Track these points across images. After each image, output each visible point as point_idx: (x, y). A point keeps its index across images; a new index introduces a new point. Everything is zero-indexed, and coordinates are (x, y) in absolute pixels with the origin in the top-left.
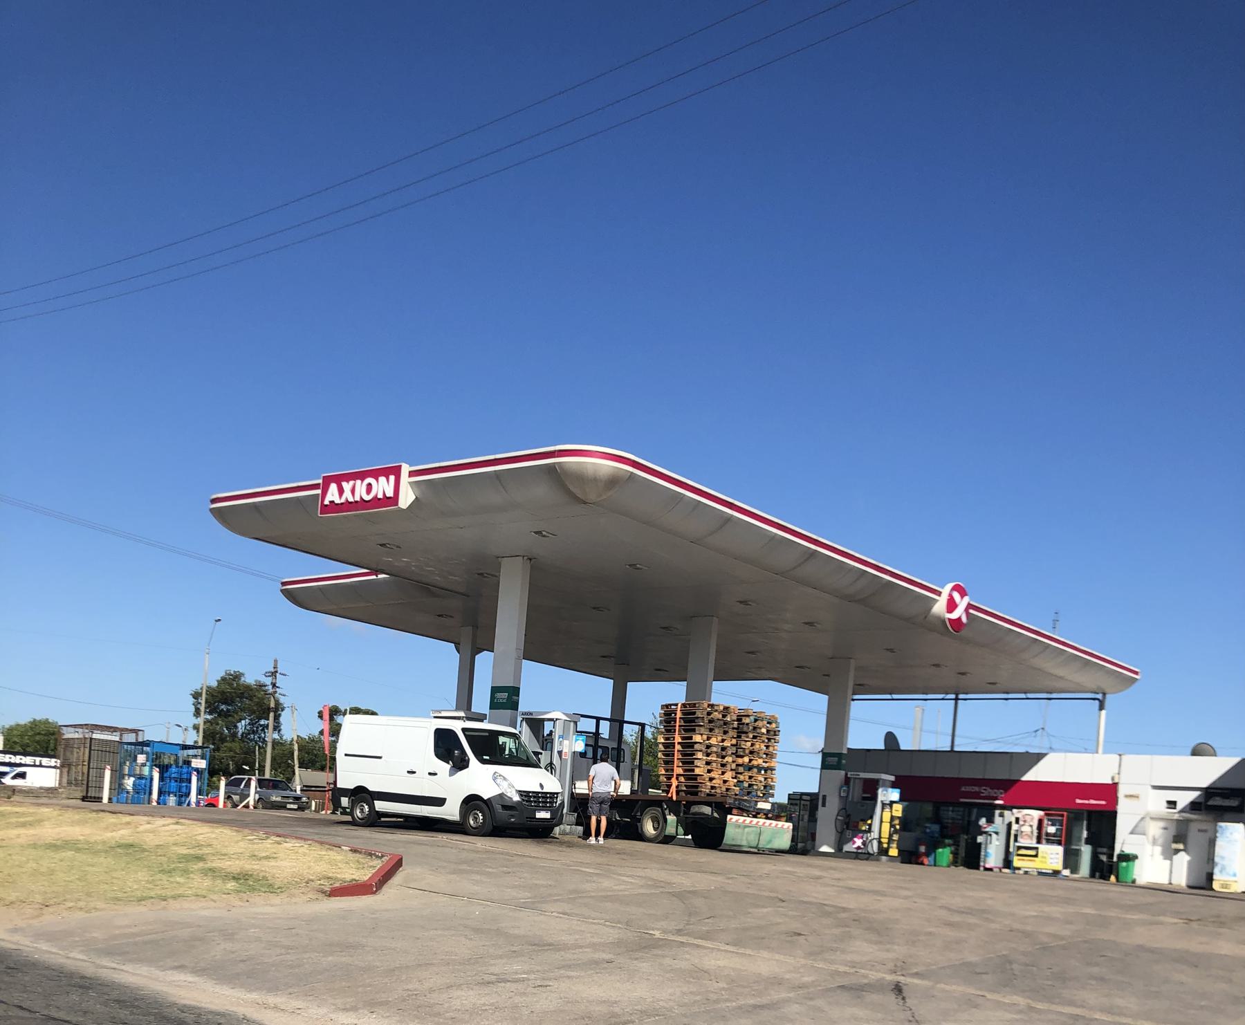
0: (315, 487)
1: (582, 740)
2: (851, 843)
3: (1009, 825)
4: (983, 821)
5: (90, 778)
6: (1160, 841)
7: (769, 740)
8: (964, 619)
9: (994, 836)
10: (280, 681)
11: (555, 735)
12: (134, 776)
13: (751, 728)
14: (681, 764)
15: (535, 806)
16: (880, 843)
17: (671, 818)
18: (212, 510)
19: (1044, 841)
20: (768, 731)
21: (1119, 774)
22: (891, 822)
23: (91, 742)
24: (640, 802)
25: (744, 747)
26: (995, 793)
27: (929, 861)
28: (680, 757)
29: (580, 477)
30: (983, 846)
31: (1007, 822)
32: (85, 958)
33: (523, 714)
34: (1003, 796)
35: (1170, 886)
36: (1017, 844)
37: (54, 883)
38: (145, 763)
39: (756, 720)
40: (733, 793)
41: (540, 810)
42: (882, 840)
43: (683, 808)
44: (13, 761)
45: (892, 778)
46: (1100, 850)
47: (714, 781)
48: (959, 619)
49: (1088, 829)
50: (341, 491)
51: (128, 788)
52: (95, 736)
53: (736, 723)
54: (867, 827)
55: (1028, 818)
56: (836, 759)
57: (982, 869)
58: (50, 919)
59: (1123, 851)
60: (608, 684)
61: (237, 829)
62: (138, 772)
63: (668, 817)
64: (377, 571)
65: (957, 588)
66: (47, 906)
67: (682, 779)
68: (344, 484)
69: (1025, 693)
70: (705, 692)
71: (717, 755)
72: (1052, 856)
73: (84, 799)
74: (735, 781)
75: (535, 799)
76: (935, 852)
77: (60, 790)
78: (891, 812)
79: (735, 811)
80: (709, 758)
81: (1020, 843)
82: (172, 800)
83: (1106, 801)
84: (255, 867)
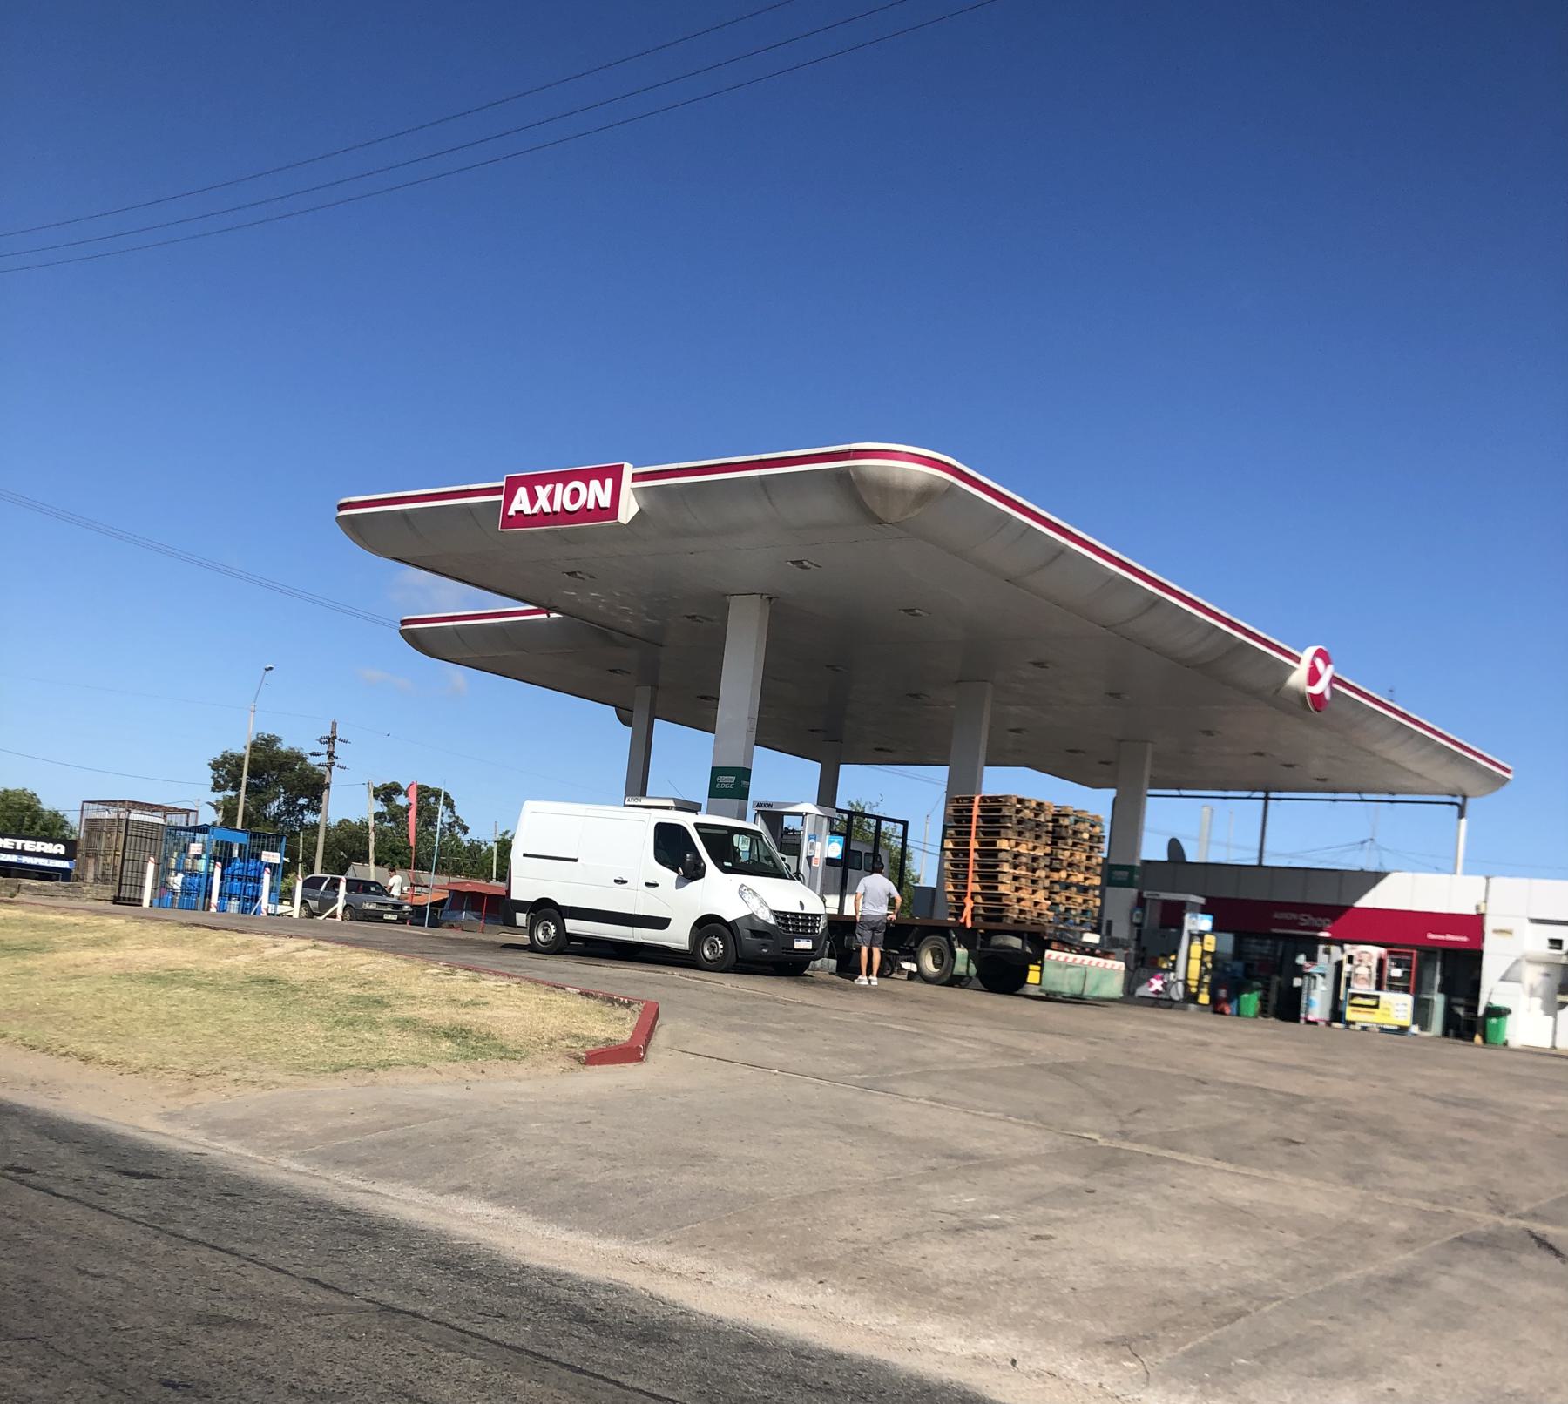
0: (497, 491)
1: (839, 842)
2: (1146, 985)
3: (1339, 965)
4: (1301, 959)
5: (124, 874)
6: (1540, 991)
7: (1092, 848)
8: (1328, 695)
9: (1320, 979)
10: (339, 749)
11: (804, 835)
12: (183, 872)
13: (1071, 832)
14: (977, 879)
15: (794, 932)
16: (1186, 986)
17: (961, 952)
18: (338, 519)
19: (1385, 987)
20: (1091, 837)
21: (1485, 902)
22: (1201, 959)
23: (127, 824)
24: (917, 928)
25: (1061, 857)
26: (1319, 922)
27: (1231, 1009)
28: (977, 869)
29: (884, 488)
30: (1305, 992)
31: (1334, 960)
32: (302, 1168)
33: (758, 805)
34: (1329, 926)
35: (1554, 1051)
36: (1350, 991)
37: (189, 1038)
38: (201, 855)
39: (1076, 822)
40: (1046, 920)
41: (799, 938)
42: (1190, 983)
43: (979, 939)
44: (45, 850)
45: (1202, 901)
46: (1455, 1000)
47: (1023, 903)
48: (1322, 695)
49: (1442, 974)
50: (533, 498)
51: (175, 887)
52: (132, 817)
53: (1050, 824)
54: (1171, 965)
55: (1365, 957)
56: (1127, 873)
57: (1302, 1021)
58: (207, 1097)
59: (1491, 1004)
60: (815, 767)
61: (405, 957)
62: (190, 867)
63: (958, 950)
64: (549, 609)
65: (1320, 654)
66: (197, 1076)
67: (979, 899)
68: (538, 489)
69: (1359, 793)
70: (975, 781)
71: (1027, 868)
72: (1399, 1008)
73: (116, 900)
74: (1049, 903)
75: (804, 924)
76: (1238, 998)
77: (84, 888)
78: (1202, 945)
79: (1054, 945)
80: (1017, 872)
81: (1353, 988)
82: (234, 905)
83: (1468, 936)
84: (468, 1017)
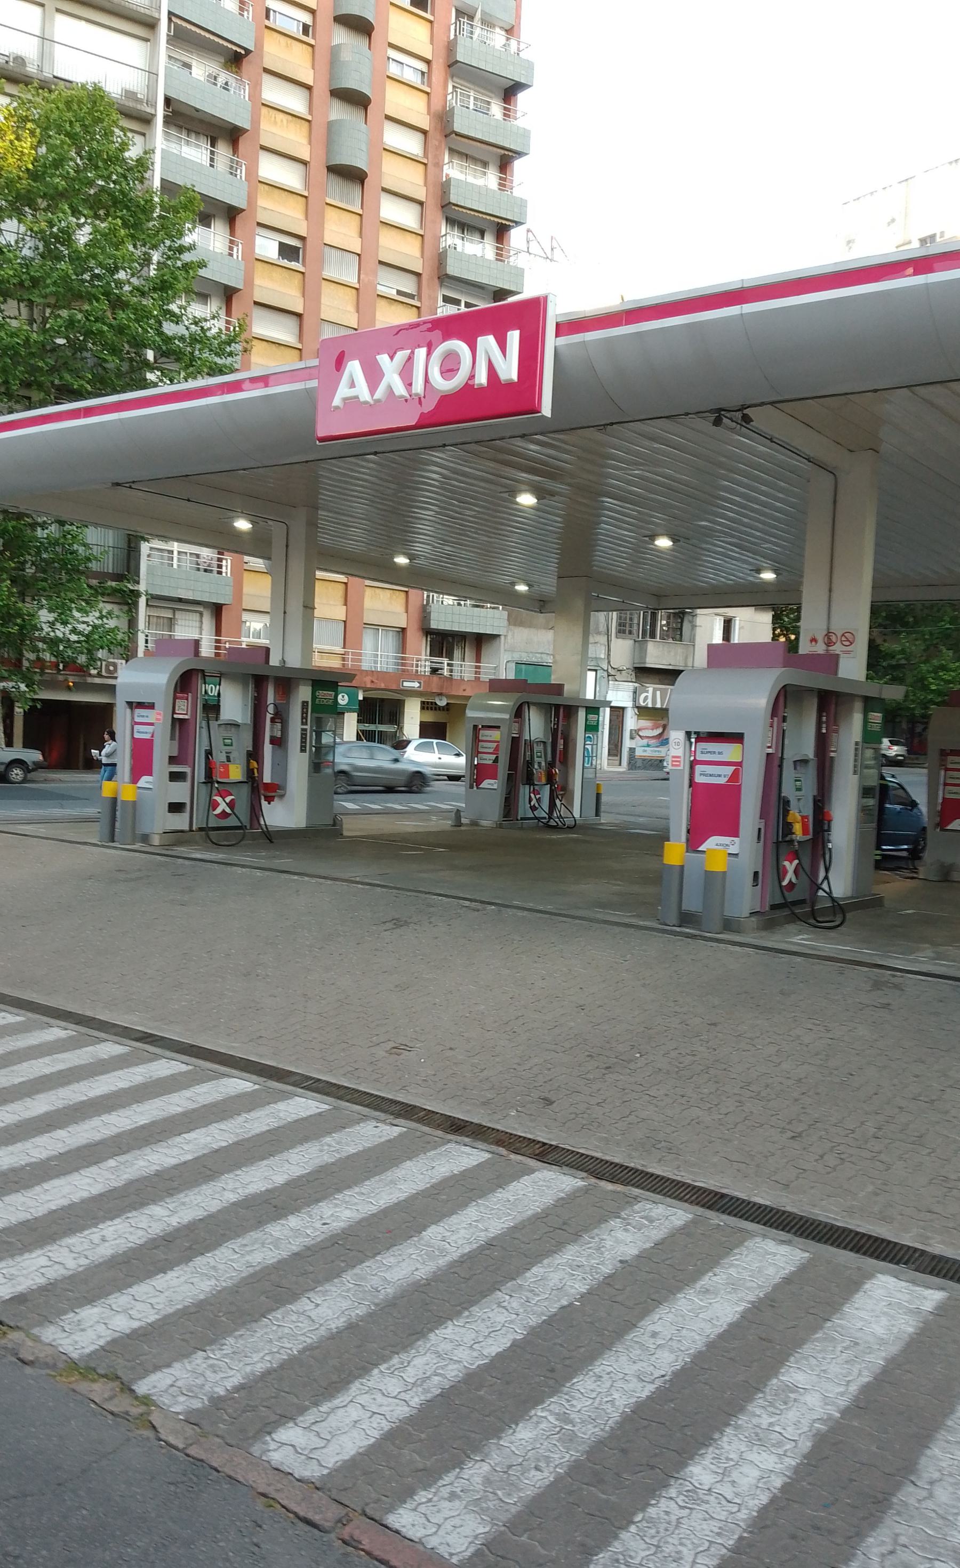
50: (373, 375)
